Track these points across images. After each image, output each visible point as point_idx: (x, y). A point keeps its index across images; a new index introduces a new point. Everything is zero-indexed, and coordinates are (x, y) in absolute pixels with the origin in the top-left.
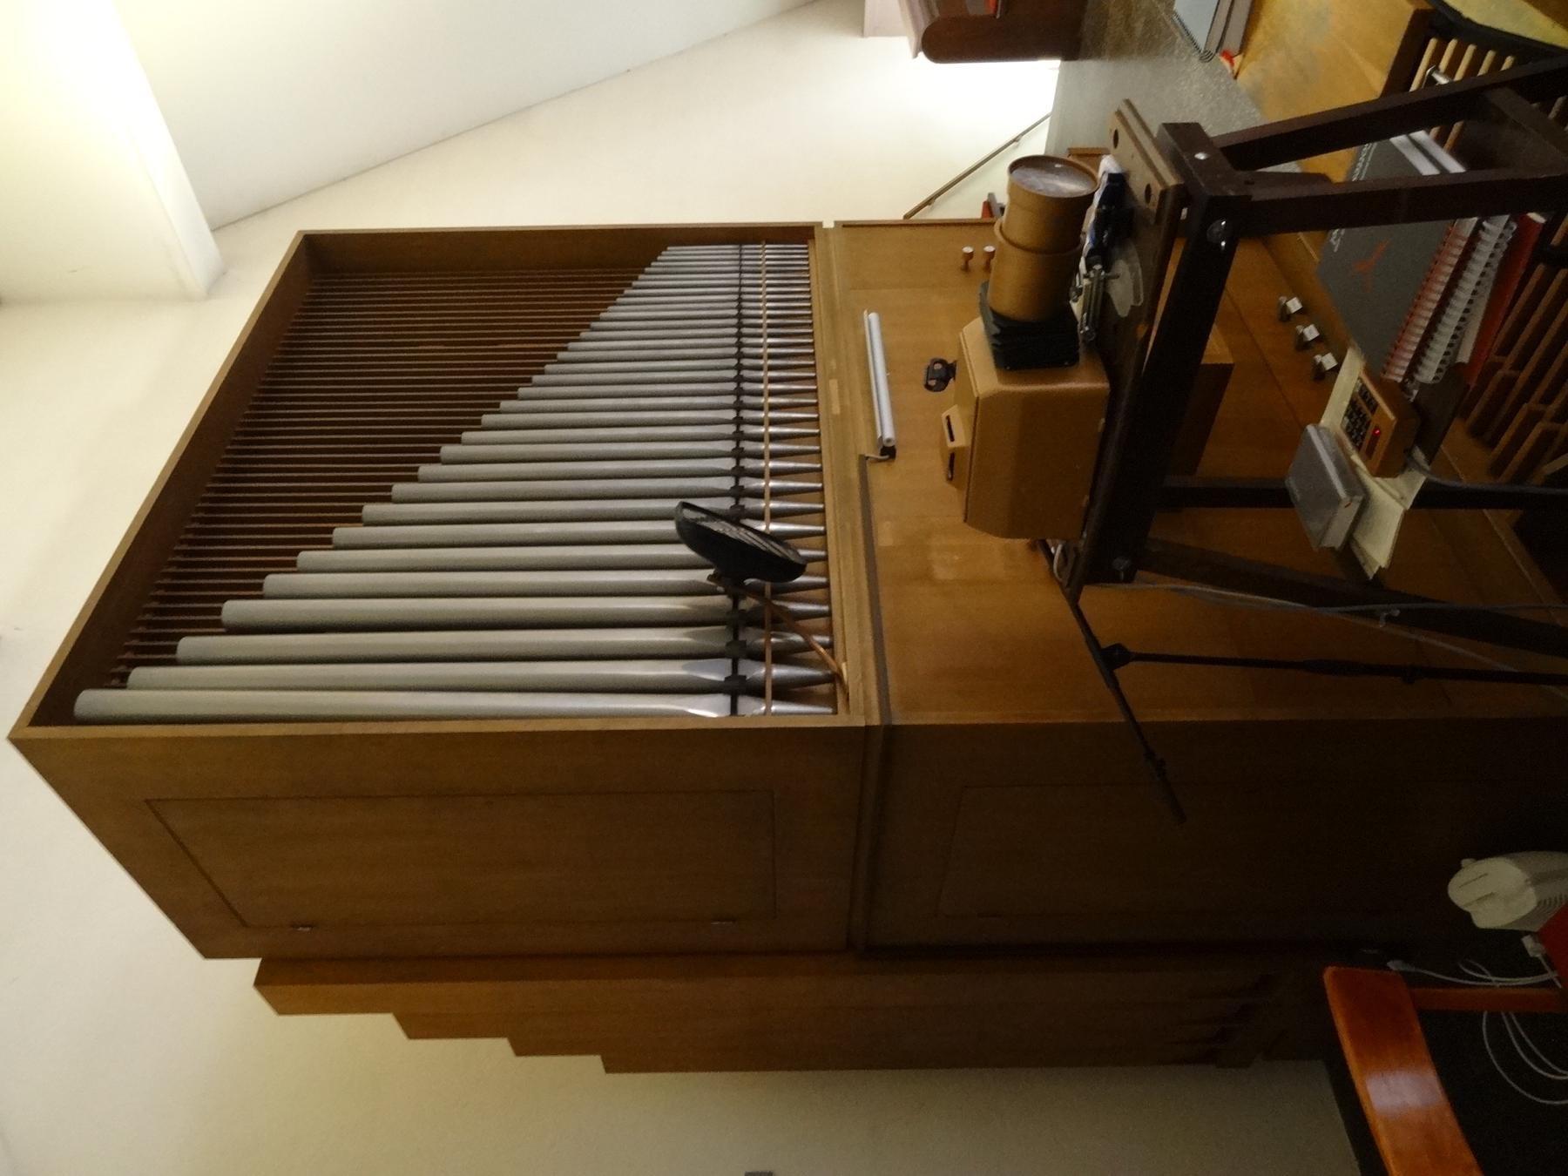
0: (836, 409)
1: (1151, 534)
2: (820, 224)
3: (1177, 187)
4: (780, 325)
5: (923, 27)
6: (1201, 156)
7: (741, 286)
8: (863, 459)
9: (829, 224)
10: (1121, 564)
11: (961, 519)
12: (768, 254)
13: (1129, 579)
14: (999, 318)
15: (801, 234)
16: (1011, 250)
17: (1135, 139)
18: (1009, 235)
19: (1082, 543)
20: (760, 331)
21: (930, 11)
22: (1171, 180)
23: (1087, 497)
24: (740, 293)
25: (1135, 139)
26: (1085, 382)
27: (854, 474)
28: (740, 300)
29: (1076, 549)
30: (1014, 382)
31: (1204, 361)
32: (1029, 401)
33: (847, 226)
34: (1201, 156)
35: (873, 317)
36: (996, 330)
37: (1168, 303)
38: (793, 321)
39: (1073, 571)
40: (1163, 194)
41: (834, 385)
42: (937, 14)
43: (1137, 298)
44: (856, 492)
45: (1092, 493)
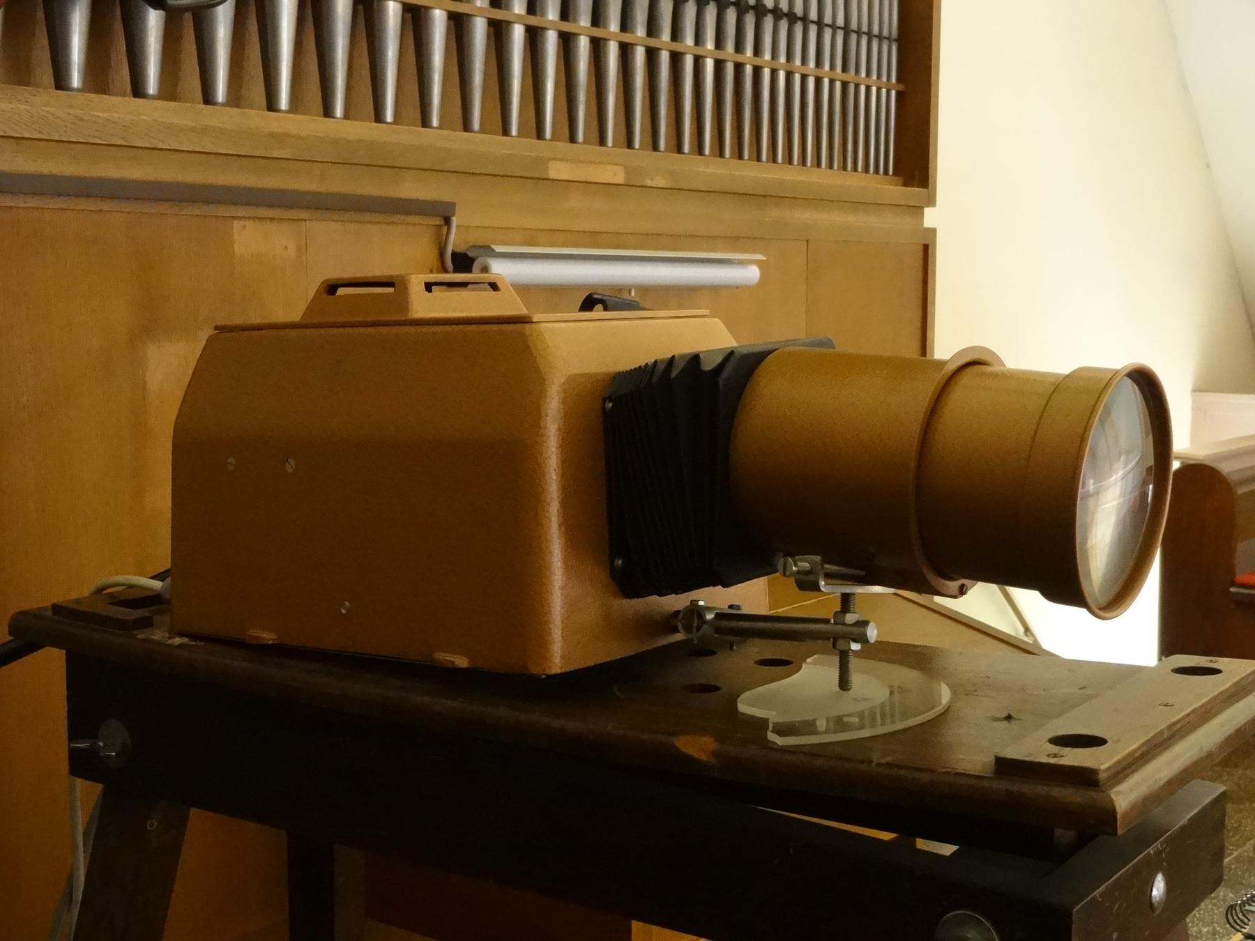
0: (558, 171)
1: (196, 815)
2: (931, 202)
3: (1110, 814)
4: (740, 87)
5: (1226, 468)
6: (1158, 889)
7: (820, 24)
8: (444, 215)
9: (930, 217)
10: (111, 742)
11: (221, 322)
12: (878, 91)
13: (81, 765)
14: (743, 368)
15: (913, 160)
16: (926, 389)
17: (1205, 714)
18: (966, 379)
19: (158, 635)
20: (730, 46)
21: (1243, 482)
22: (1124, 797)
23: (268, 637)
24: (805, 19)
25: (1205, 714)
26: (569, 613)
27: (411, 189)
28: (792, 18)
29: (146, 623)
30: (569, 414)
31: (636, 925)
32: (516, 457)
33: (926, 253)
34: (1158, 889)
35: (752, 274)
36: (708, 366)
37: (745, 252)
38: (744, 119)
39: (105, 621)
40: (1085, 778)
41: (615, 175)
42: (1241, 491)
43: (782, 730)
44: (370, 188)
45: (278, 651)
